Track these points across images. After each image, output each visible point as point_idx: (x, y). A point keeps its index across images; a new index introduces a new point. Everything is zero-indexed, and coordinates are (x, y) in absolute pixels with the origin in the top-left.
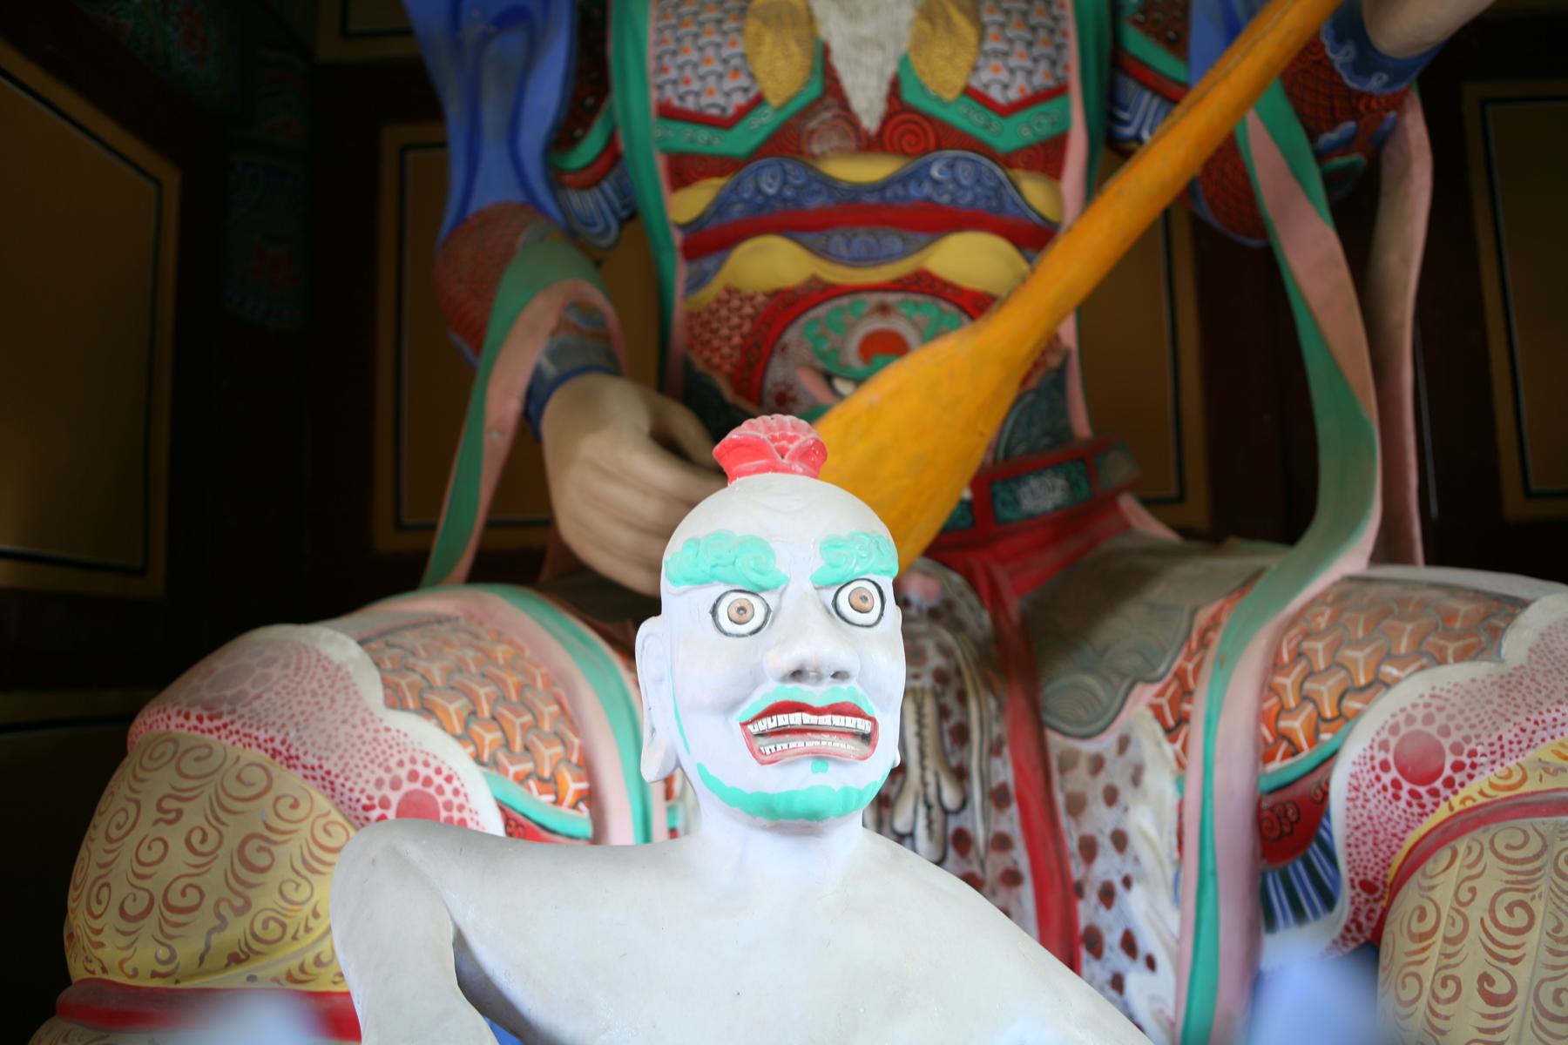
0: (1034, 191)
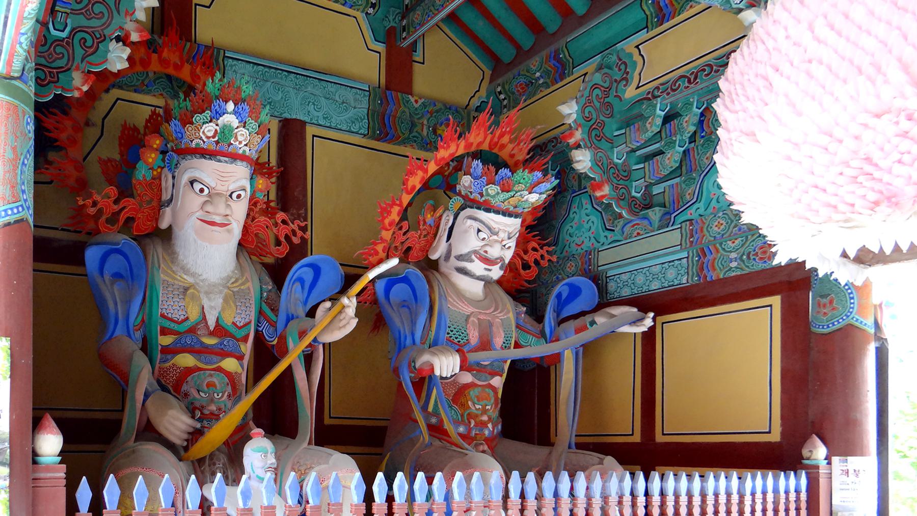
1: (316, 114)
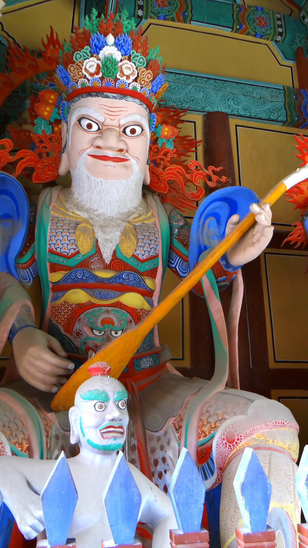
0: (149, 282)
1: (236, 107)
